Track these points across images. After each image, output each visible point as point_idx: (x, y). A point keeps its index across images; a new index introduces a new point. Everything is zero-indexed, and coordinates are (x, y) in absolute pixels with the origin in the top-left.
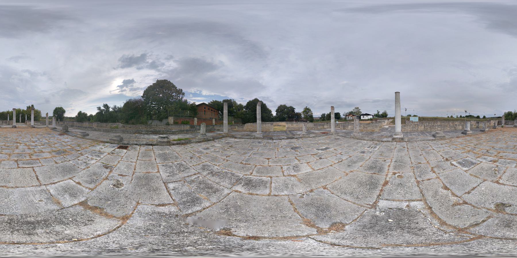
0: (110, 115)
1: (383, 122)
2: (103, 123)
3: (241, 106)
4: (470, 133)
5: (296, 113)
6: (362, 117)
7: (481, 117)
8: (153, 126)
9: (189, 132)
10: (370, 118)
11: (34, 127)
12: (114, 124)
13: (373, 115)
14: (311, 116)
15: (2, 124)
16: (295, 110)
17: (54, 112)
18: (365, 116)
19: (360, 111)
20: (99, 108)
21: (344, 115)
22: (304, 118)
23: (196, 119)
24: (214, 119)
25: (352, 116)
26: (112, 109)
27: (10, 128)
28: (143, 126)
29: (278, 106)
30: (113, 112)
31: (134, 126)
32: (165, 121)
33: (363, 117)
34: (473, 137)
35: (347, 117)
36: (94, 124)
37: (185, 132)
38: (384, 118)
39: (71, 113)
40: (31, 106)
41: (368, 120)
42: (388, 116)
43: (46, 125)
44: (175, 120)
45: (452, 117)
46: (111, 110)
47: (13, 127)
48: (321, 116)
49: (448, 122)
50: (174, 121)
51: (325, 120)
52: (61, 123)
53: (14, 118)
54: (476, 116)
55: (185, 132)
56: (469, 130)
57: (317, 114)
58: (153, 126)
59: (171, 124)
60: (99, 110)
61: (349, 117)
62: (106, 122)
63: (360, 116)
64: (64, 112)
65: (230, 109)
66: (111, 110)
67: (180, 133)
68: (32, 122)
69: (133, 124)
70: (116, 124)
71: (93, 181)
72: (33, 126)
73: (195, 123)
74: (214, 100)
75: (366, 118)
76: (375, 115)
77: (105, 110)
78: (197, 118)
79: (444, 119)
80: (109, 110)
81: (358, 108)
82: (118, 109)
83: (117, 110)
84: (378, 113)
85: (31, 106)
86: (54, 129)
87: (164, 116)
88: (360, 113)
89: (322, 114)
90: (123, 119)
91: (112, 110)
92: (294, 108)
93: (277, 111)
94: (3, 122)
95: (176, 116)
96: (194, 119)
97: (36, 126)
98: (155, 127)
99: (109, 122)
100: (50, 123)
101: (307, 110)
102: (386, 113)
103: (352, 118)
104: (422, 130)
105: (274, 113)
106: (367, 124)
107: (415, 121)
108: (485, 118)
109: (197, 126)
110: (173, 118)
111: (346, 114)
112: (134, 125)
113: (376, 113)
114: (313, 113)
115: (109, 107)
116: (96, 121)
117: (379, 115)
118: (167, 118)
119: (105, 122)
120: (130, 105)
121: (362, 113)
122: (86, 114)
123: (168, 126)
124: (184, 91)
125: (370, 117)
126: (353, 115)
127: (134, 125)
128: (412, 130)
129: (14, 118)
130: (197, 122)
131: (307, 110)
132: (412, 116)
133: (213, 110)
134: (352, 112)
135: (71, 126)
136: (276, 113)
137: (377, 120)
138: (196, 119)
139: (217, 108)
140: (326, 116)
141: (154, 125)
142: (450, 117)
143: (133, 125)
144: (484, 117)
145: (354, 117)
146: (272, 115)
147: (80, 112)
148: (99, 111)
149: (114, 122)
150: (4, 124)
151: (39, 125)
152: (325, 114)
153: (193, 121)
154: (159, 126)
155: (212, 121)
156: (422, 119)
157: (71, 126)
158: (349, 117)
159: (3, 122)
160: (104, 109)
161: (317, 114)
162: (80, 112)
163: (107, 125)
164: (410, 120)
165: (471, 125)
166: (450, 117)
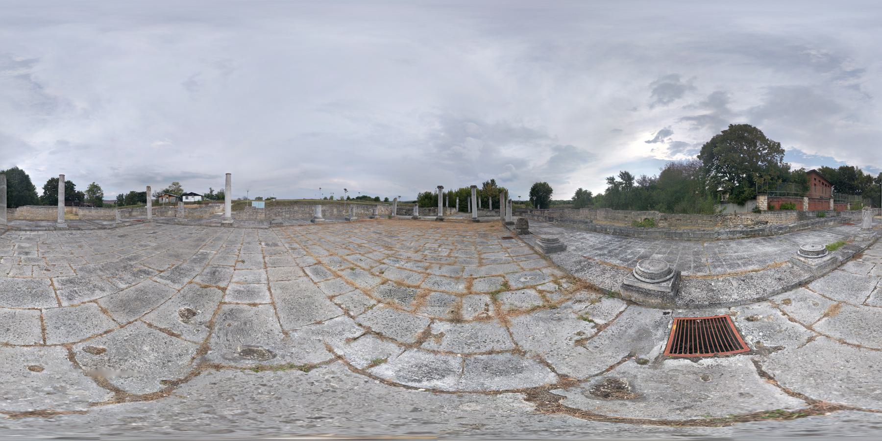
0: (633, 193)
1: (217, 208)
2: (617, 211)
3: (869, 178)
4: (321, 221)
5: (76, 192)
6: (184, 197)
7: (382, 199)
8: (729, 217)
9: (816, 226)
10: (197, 200)
11: (478, 221)
12: (645, 214)
13: (202, 196)
15: (429, 213)
16: (75, 187)
18: (189, 197)
19: (180, 188)
20: (611, 180)
23: (806, 199)
24: (833, 200)
25: (168, 196)
26: (638, 182)
27: (432, 220)
28: (705, 219)
29: (48, 180)
30: (642, 189)
31: (688, 216)
32: (750, 205)
33: (187, 198)
34: (163, 230)
35: (160, 199)
36: (598, 211)
37: (810, 227)
38: (220, 201)
39: (563, 193)
41: (195, 203)
43: (499, 216)
44: (771, 201)
45: (332, 198)
46: (636, 184)
47: (436, 220)
48: (117, 198)
49: (309, 206)
50: (769, 204)
51: (124, 205)
53: (440, 204)
54: (374, 197)
55: (810, 227)
56: (321, 216)
57: (110, 194)
58: (729, 217)
59: (765, 211)
60: (610, 183)
61: (164, 199)
62: (626, 210)
63: (182, 196)
64: (549, 191)
65: (853, 183)
66: (636, 184)
67: (802, 230)
68: (475, 213)
69: (684, 211)
70: (647, 212)
71: (229, 314)
72: (476, 218)
73: (804, 207)
74: (825, 167)
75: (191, 199)
76: (205, 196)
77: (623, 184)
78: (807, 198)
79: (288, 202)
80: (631, 184)
81: (178, 183)
82: (650, 184)
83: (649, 187)
84: (211, 192)
85: (490, 182)
87: (750, 195)
88: (180, 192)
89: (118, 196)
90: (663, 203)
91: (638, 185)
92: (74, 185)
93: (46, 188)
94: (430, 210)
95: (771, 195)
96: (803, 199)
97: (480, 219)
98: (733, 217)
99: (632, 209)
101: (94, 189)
102: (223, 193)
103: (167, 200)
104: (262, 218)
105: (40, 192)
106: (193, 209)
107: (259, 207)
108: (388, 201)
109: (809, 213)
110: (766, 198)
111: (157, 194)
112: (688, 215)
113: (208, 192)
114: (103, 193)
115: (633, 176)
116: (603, 207)
117: (213, 195)
118: (754, 198)
119: (623, 209)
120: (671, 173)
121: (185, 191)
122: (590, 194)
123: (758, 215)
124: (783, 146)
125: (197, 198)
126: (170, 196)
127: (687, 213)
128: (249, 219)
129: (440, 204)
130: (807, 205)
131: (94, 189)
132: (264, 199)
133: (825, 183)
134: (168, 190)
135: (549, 218)
136: (44, 191)
137: (208, 204)
138: (806, 199)
139: (830, 180)
140: (124, 197)
141: (731, 215)
142: (328, 198)
143: (685, 215)
144: (386, 200)
145: (171, 198)
146: (36, 194)
147: (580, 190)
148: (611, 185)
149: (644, 210)
150: (432, 214)
151: (493, 216)
152: (123, 194)
153: (802, 203)
154: (742, 215)
155: (829, 203)
156: (271, 203)
157: (549, 218)
158: (162, 199)
159: (430, 210)
160: (621, 181)
161: (110, 194)
162: (580, 190)
163: (626, 215)
164: (253, 206)
165: (323, 211)
166: (328, 198)
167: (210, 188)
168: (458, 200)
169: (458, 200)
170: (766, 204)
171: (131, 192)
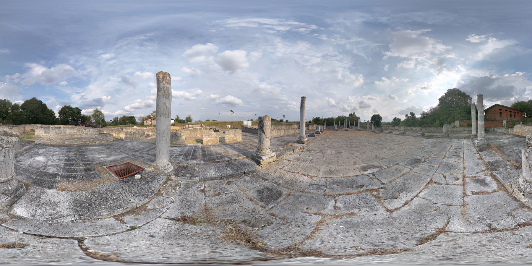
5: (82, 115)
11: (360, 131)
14: (103, 121)
16: (81, 112)
17: (371, 119)
21: (139, 120)
22: (96, 122)
32: (452, 125)
35: (145, 122)
40: (352, 113)
42: (193, 122)
50: (460, 124)
51: (118, 125)
52: (378, 128)
54: (279, 120)
59: (458, 127)
61: (148, 121)
70: (416, 127)
85: (352, 113)
86: (373, 131)
93: (59, 113)
100: (370, 128)
103: (150, 123)
105: (57, 115)
122: (400, 120)
131: (98, 114)
140: (118, 119)
144: (376, 120)
146: (55, 117)
147: (396, 118)
162: (396, 118)
167: (177, 116)
168: (340, 122)
169: (340, 122)
170: (458, 124)
171: (440, 100)
